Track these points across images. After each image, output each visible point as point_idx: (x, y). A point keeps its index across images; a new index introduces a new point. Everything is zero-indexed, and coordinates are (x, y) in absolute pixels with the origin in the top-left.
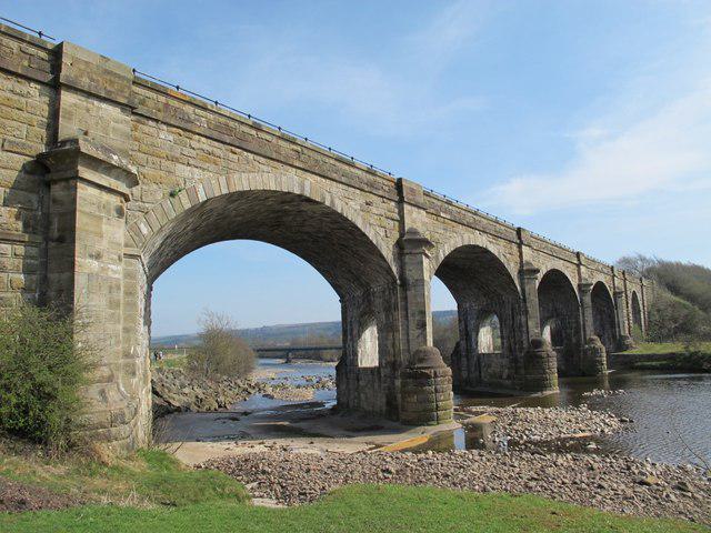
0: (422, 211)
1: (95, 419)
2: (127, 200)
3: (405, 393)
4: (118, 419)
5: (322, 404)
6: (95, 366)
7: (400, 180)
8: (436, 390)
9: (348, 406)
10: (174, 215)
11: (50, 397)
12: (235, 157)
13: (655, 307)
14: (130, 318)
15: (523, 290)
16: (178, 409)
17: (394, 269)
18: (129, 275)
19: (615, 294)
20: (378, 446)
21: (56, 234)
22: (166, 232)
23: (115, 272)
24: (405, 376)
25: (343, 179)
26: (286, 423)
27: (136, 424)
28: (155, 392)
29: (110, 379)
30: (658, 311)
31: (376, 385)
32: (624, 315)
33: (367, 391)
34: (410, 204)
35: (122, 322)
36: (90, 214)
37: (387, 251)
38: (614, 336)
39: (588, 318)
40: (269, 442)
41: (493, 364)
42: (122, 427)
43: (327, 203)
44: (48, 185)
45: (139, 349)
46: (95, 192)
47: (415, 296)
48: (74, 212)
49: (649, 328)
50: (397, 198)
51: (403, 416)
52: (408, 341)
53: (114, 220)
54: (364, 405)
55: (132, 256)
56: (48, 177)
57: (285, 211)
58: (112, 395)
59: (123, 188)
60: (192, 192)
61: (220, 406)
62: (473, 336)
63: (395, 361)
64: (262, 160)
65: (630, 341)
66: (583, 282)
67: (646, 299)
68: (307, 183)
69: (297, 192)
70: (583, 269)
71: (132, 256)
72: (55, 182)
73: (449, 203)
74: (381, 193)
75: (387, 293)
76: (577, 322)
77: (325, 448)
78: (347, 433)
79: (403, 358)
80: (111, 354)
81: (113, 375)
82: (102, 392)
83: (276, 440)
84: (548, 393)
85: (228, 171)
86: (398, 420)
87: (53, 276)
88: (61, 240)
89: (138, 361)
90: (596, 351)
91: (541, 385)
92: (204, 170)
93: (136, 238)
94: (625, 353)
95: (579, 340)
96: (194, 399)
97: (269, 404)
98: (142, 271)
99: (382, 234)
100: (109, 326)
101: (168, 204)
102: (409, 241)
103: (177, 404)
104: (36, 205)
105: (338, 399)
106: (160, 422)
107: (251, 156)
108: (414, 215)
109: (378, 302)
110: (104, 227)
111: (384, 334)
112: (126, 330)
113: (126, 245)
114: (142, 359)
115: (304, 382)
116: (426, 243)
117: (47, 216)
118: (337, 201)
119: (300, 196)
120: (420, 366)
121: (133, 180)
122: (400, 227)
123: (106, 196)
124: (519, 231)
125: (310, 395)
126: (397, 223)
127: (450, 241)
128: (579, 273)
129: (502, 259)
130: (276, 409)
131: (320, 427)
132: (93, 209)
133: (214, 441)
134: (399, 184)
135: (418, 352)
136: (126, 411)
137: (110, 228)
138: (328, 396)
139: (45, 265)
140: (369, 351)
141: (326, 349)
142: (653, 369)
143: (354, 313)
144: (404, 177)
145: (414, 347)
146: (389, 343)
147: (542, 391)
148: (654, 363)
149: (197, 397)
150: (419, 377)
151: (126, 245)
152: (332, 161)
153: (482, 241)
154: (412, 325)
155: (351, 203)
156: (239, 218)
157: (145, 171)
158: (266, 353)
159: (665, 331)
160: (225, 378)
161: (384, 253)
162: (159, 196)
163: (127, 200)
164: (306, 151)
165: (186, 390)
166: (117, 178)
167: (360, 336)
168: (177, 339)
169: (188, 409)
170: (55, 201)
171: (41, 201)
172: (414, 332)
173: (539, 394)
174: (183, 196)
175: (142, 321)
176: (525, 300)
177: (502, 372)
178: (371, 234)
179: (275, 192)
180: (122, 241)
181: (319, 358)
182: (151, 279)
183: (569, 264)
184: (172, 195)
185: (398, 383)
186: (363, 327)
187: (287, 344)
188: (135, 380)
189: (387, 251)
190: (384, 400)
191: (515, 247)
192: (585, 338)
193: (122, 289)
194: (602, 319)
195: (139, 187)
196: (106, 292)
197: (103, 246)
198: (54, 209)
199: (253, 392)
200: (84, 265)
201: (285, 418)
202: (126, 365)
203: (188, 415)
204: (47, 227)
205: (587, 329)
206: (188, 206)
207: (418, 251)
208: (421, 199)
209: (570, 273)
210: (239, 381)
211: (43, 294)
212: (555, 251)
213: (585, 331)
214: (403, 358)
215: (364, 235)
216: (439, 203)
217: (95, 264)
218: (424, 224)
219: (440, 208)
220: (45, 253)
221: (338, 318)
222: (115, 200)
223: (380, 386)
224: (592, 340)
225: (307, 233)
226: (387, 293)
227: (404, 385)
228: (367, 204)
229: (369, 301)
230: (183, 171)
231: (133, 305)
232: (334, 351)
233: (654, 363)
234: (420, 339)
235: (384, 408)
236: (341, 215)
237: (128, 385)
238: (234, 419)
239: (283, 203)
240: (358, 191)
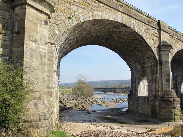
0: (167, 34)
1: (31, 118)
2: (50, 18)
3: (160, 107)
4: (43, 117)
5: (121, 109)
6: (32, 92)
7: (159, 21)
8: (174, 108)
9: (133, 110)
10: (70, 27)
11: (9, 106)
12: (96, 4)
14: (50, 71)
16: (69, 108)
17: (157, 57)
18: (50, 52)
20: (151, 130)
21: (16, 30)
22: (66, 36)
23: (44, 49)
24: (161, 101)
25: (138, 19)
26: (109, 116)
27: (52, 118)
28: (60, 102)
29: (40, 98)
31: (146, 104)
33: (142, 105)
34: (162, 30)
35: (46, 72)
36: (32, 21)
37: (155, 49)
40: (105, 124)
42: (44, 121)
43: (132, 28)
44: (13, 8)
45: (54, 85)
46: (35, 11)
47: (165, 68)
48: (25, 19)
50: (158, 28)
51: (159, 117)
52: (162, 86)
53: (44, 26)
54: (140, 111)
55: (51, 43)
56: (13, 4)
57: (114, 31)
58: (41, 106)
59: (47, 12)
60: (78, 18)
61: (83, 108)
62: (179, 86)
63: (156, 94)
64: (107, 7)
68: (124, 19)
69: (120, 22)
71: (51, 43)
72: (16, 6)
73: (177, 32)
74: (152, 25)
75: (153, 67)
77: (128, 129)
78: (135, 122)
79: (160, 93)
80: (40, 87)
81: (41, 97)
82: (36, 105)
83: (108, 124)
85: (92, 10)
86: (157, 118)
87: (15, 49)
88: (18, 33)
89: (53, 91)
92: (83, 8)
93: (53, 36)
96: (74, 105)
97: (100, 108)
98: (56, 51)
99: (153, 42)
100: (40, 74)
101: (67, 21)
102: (163, 46)
103: (68, 106)
104: (8, 17)
105: (128, 107)
106: (63, 113)
107: (102, 5)
108: (165, 35)
109: (148, 71)
110: (39, 28)
111: (151, 84)
112: (48, 76)
113: (49, 39)
114: (55, 90)
115: (111, 100)
116: (170, 46)
117: (13, 22)
118: (136, 27)
119: (121, 24)
120: (167, 97)
121: (53, 11)
122: (159, 40)
123: (40, 15)
125: (114, 105)
126: (158, 38)
130: (104, 110)
131: (123, 119)
132: (33, 19)
133: (84, 123)
134: (159, 23)
135: (166, 91)
136: (47, 114)
137: (42, 29)
138: (124, 106)
139: (11, 44)
140: (143, 89)
141: (117, 89)
143: (136, 75)
144: (161, 20)
145: (165, 89)
146: (153, 87)
149: (75, 104)
150: (167, 102)
151: (49, 39)
152: (134, 11)
153: (125, 20)
154: (164, 80)
155: (141, 28)
156: (95, 34)
157: (57, 6)
158: (98, 89)
160: (85, 97)
161: (153, 50)
162: (64, 18)
163: (50, 18)
164: (124, 5)
165: (72, 102)
166: (45, 7)
167: (139, 84)
168: (68, 84)
169: (72, 108)
170: (16, 15)
171: (10, 16)
172: (165, 83)
174: (74, 19)
175: (55, 73)
178: (148, 42)
179: (112, 21)
180: (47, 36)
181: (115, 92)
182: (60, 58)
184: (69, 18)
185: (157, 103)
186: (140, 80)
187: (104, 87)
188: (52, 99)
189: (155, 49)
190: (150, 110)
193: (47, 57)
195: (55, 13)
196: (39, 57)
197: (38, 37)
198: (16, 19)
199: (94, 103)
200: (29, 45)
201: (109, 114)
202: (48, 92)
203: (73, 111)
204: (13, 27)
206: (76, 23)
207: (167, 50)
208: (167, 30)
210: (89, 99)
211: (10, 58)
214: (160, 93)
215: (146, 42)
216: (173, 32)
217: (34, 45)
218: (168, 39)
220: (12, 39)
221: (130, 79)
222: (44, 17)
223: (148, 104)
225: (121, 42)
226: (153, 67)
227: (160, 104)
228: (147, 29)
229: (144, 70)
230: (73, 8)
231: (51, 65)
232: (120, 90)
234: (167, 86)
235: (150, 113)
236: (137, 33)
237: (49, 101)
238: (89, 113)
239: (113, 27)
240: (144, 24)
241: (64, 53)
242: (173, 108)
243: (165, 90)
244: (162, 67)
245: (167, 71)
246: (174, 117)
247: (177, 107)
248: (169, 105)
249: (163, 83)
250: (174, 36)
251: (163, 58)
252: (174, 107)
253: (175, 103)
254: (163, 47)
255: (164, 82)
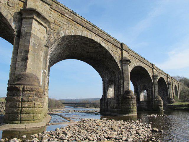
13: (183, 91)
15: (122, 69)
17: (120, 68)
19: (168, 83)
30: (184, 92)
32: (172, 91)
34: (124, 50)
38: (168, 98)
39: (156, 89)
41: (112, 103)
47: (24, 42)
49: (180, 98)
50: (121, 48)
65: (173, 100)
66: (154, 75)
67: (180, 88)
70: (154, 70)
76: (152, 90)
84: (131, 115)
90: (159, 101)
91: (129, 111)
94: (171, 104)
95: (152, 97)
119: (81, 36)
124: (122, 44)
127: (135, 63)
128: (153, 72)
129: (111, 52)
134: (167, 74)
141: (86, 104)
142: (181, 110)
147: (128, 114)
148: (182, 108)
152: (85, 22)
153: (86, 34)
159: (186, 99)
173: (127, 115)
176: (123, 73)
177: (114, 105)
183: (149, 67)
191: (119, 50)
192: (155, 96)
194: (163, 92)
205: (156, 93)
207: (30, 16)
209: (149, 70)
212: (141, 59)
213: (155, 93)
219: (135, 55)
224: (157, 97)
233: (182, 108)
241: (52, 63)
242: (20, 101)
243: (18, 74)
244: (20, 39)
245: (25, 46)
246: (21, 116)
247: (28, 99)
248: (14, 95)
249: (18, 63)
250: (65, 15)
251: (24, 27)
252: (22, 99)
253: (26, 92)
254: (125, 61)
255: (19, 62)
